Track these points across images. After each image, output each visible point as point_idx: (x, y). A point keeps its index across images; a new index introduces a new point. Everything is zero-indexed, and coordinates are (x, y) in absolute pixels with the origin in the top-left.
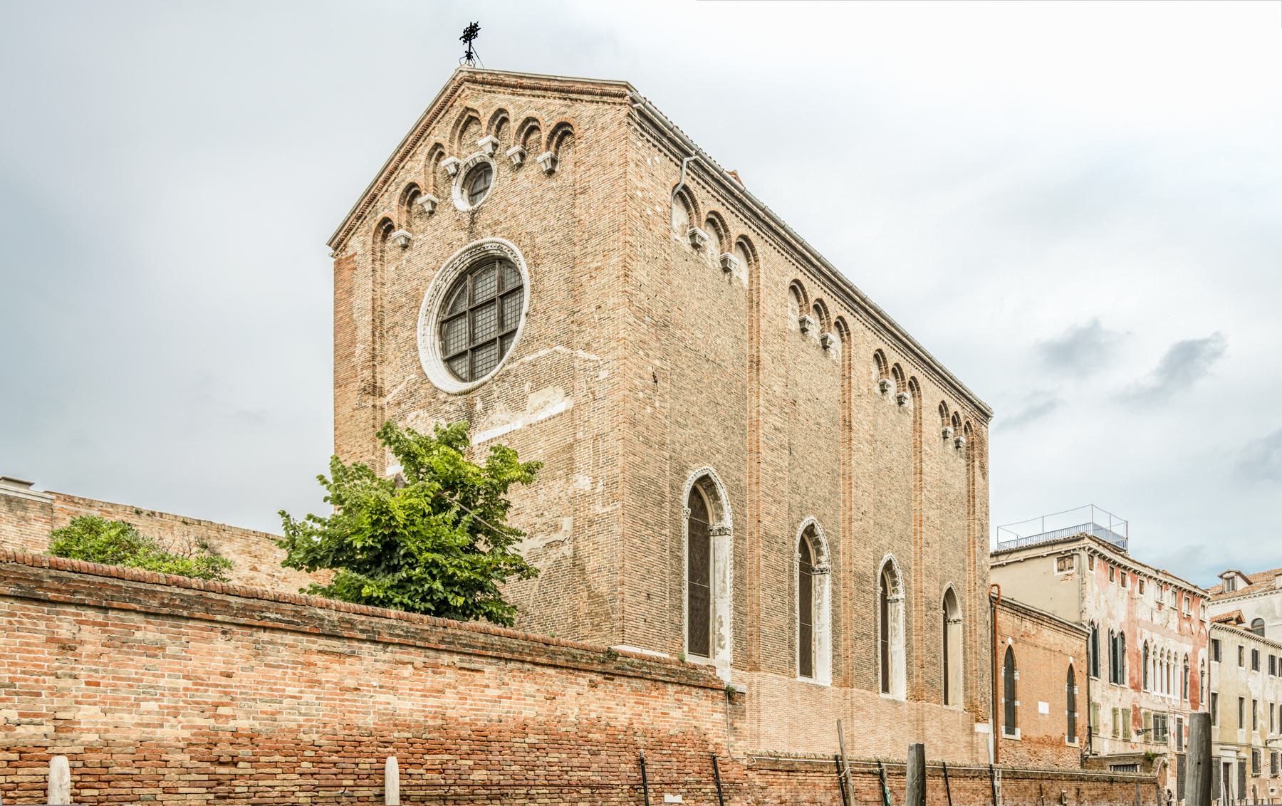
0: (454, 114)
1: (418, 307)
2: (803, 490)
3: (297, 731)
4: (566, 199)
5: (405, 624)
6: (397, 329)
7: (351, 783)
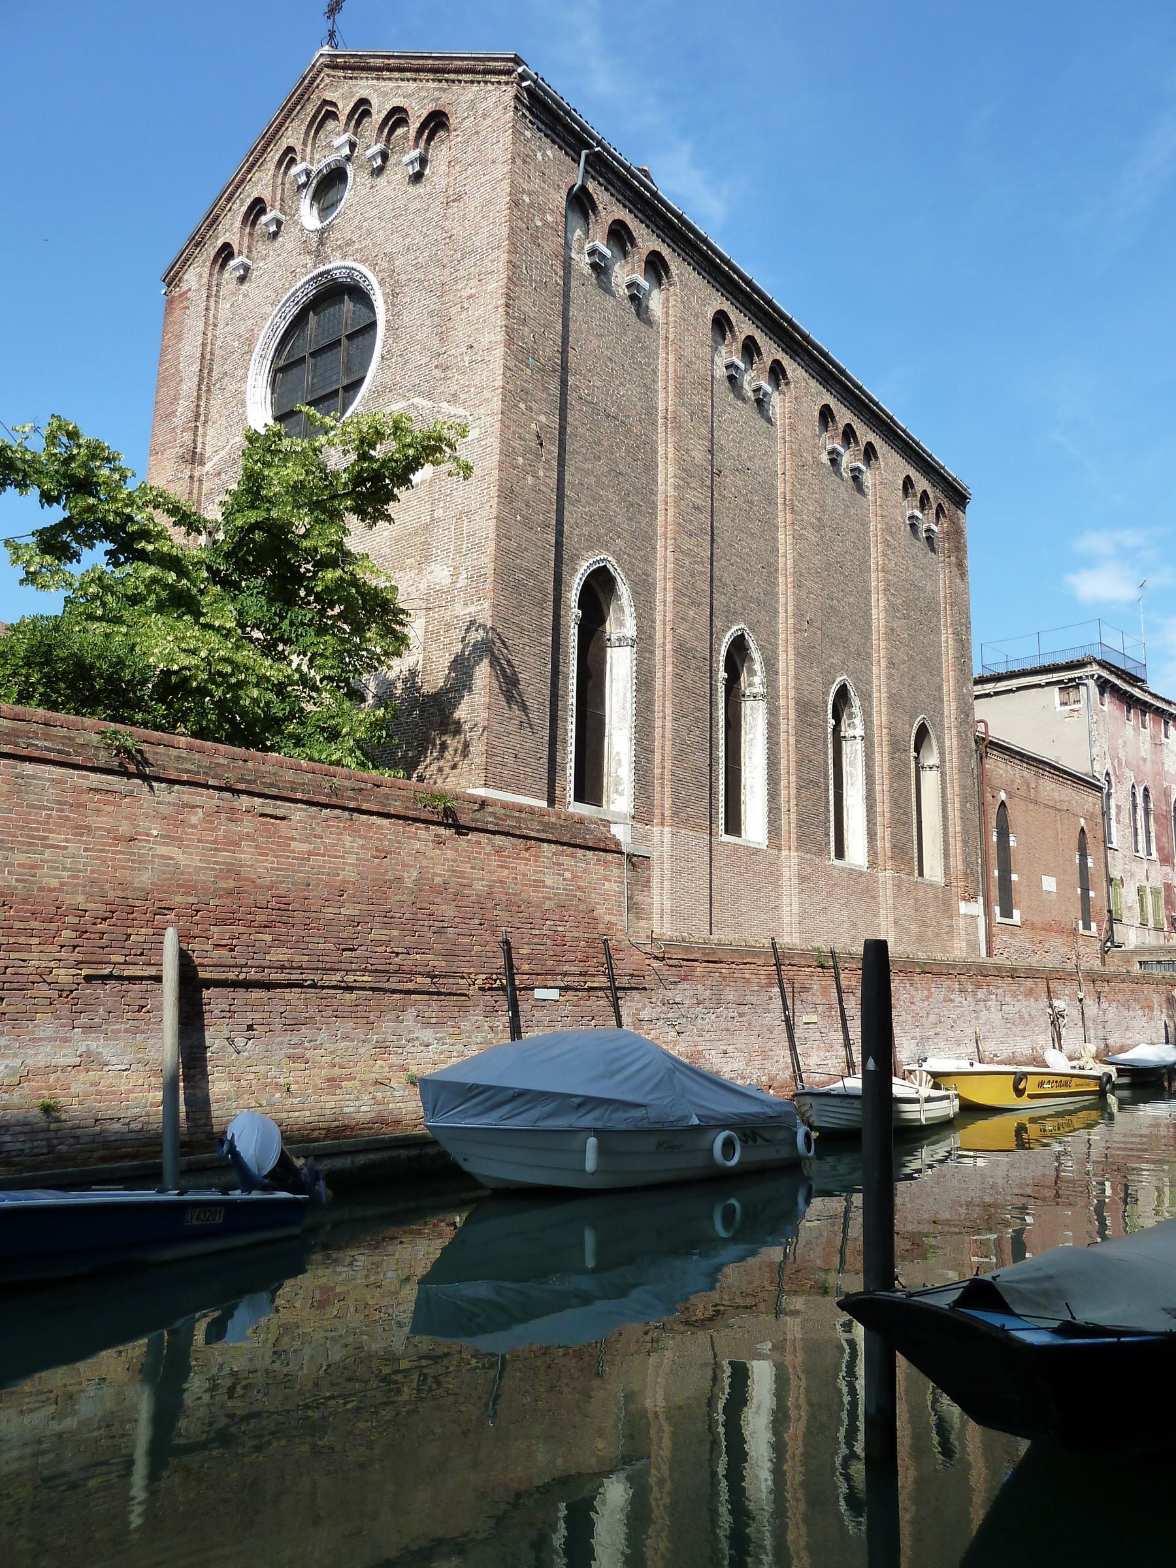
0: (311, 109)
1: (250, 352)
2: (730, 589)
3: (59, 890)
4: (437, 207)
5: (197, 756)
6: (226, 379)
7: (121, 959)
